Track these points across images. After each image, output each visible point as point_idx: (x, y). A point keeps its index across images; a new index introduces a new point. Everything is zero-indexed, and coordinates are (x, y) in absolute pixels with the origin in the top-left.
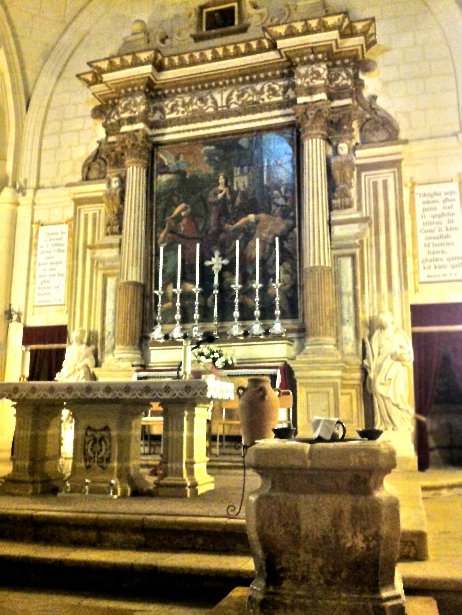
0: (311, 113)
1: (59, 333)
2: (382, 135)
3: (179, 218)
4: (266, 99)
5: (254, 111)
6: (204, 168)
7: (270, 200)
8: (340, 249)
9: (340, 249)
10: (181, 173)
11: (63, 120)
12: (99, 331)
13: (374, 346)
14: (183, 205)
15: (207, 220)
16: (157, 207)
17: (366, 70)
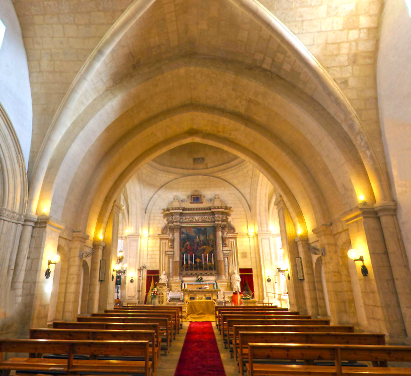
0: (219, 226)
1: (156, 272)
2: (232, 231)
3: (187, 245)
4: (207, 220)
5: (205, 222)
6: (193, 234)
7: (209, 243)
8: (225, 255)
9: (225, 255)
10: (187, 234)
11: (154, 217)
12: (356, 364)
13: (233, 278)
14: (188, 242)
15: (194, 246)
16: (183, 242)
17: (229, 216)
